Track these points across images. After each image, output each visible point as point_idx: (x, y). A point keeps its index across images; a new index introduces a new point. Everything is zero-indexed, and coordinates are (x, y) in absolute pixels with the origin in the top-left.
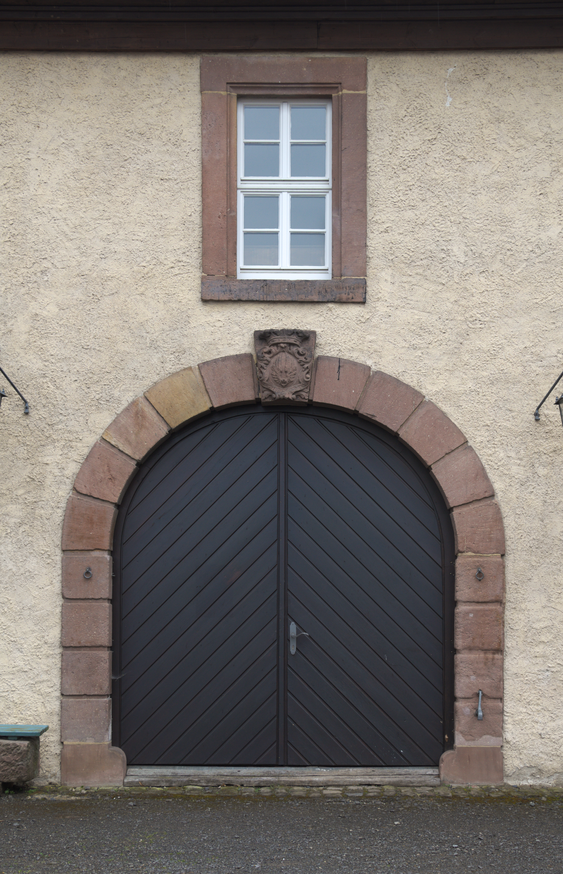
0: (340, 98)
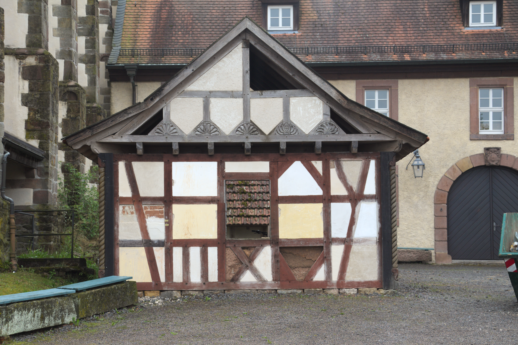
0: (507, 88)
